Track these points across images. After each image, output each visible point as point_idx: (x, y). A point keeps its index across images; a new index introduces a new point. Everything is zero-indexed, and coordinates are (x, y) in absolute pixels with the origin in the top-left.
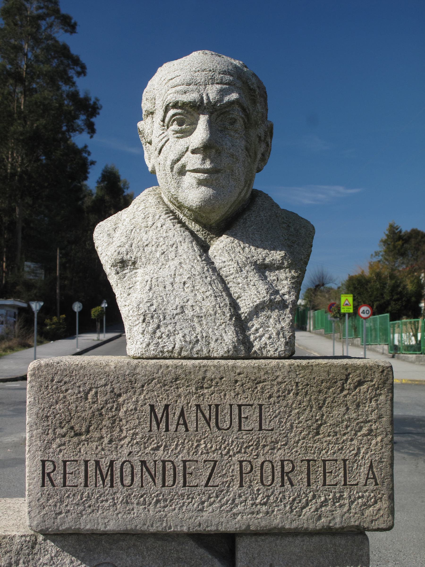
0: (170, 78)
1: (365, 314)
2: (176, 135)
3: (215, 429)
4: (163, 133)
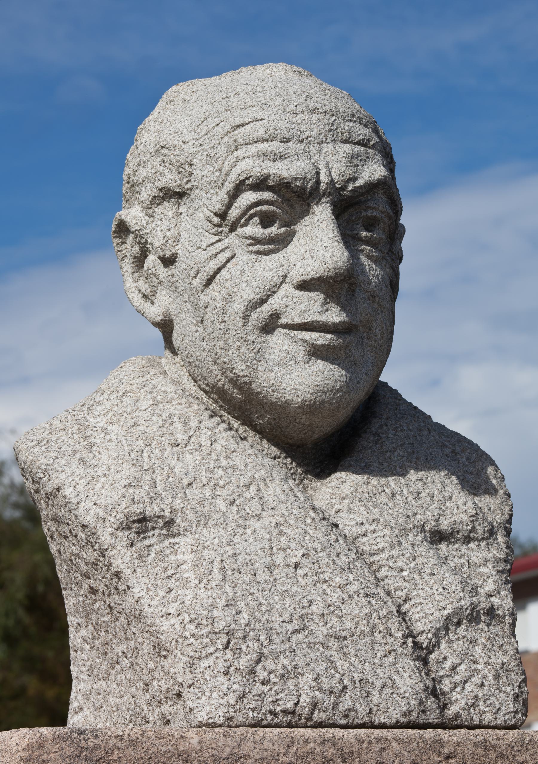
2: (255, 248)
4: (219, 241)
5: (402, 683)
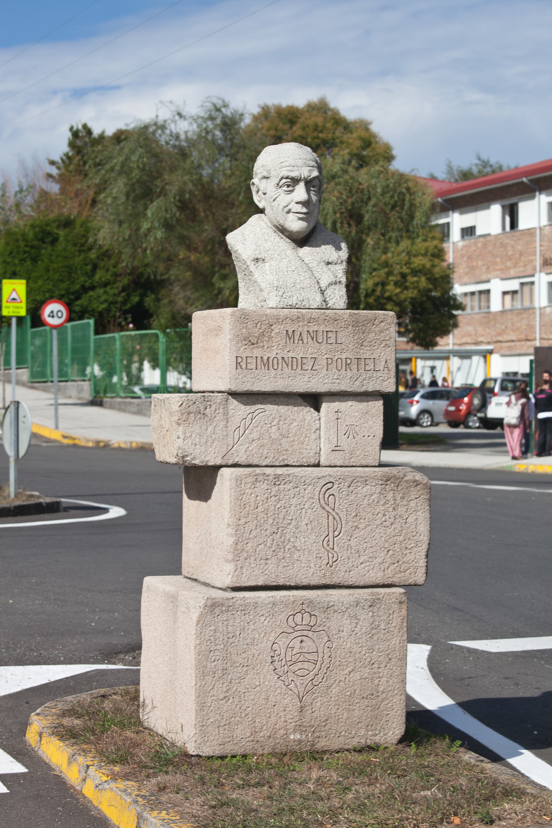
1: (56, 318)
3: (316, 343)
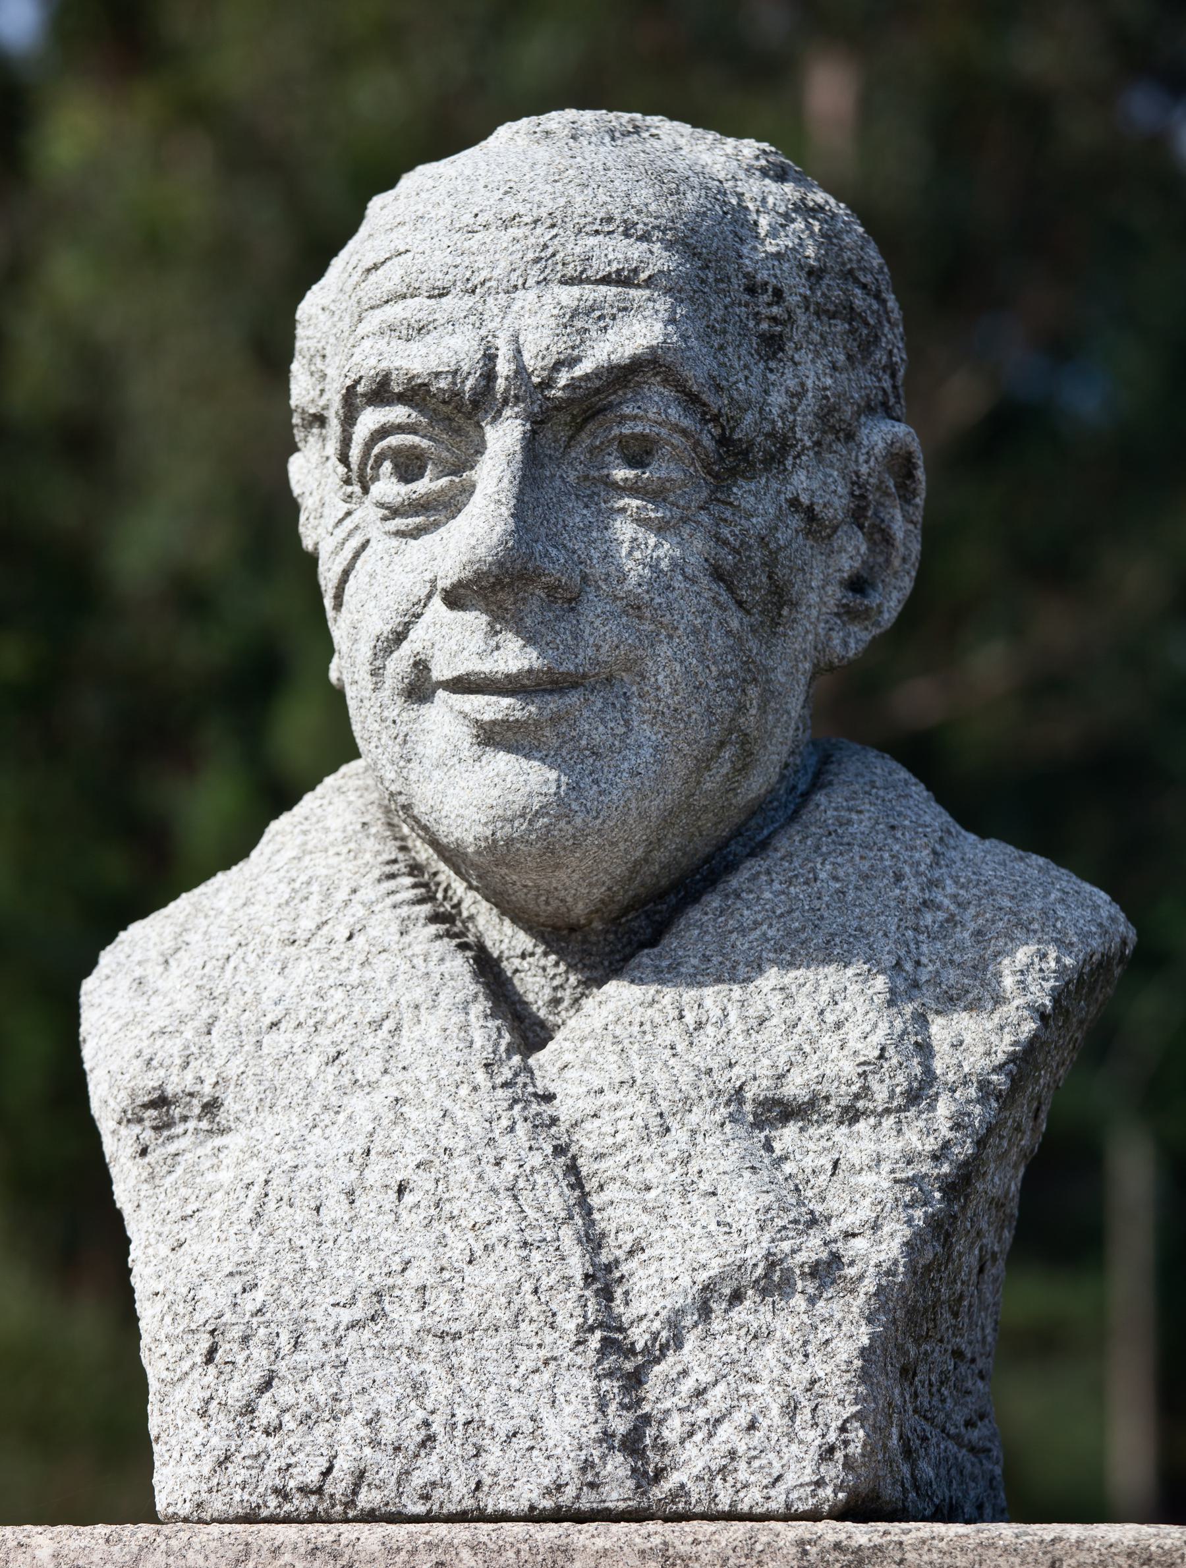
0: (370, 264)
4: (349, 514)
5: (554, 1426)
